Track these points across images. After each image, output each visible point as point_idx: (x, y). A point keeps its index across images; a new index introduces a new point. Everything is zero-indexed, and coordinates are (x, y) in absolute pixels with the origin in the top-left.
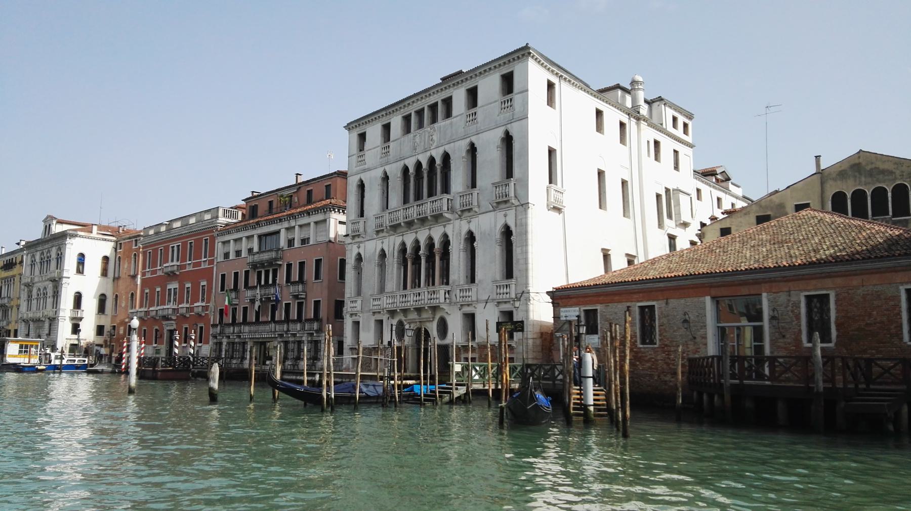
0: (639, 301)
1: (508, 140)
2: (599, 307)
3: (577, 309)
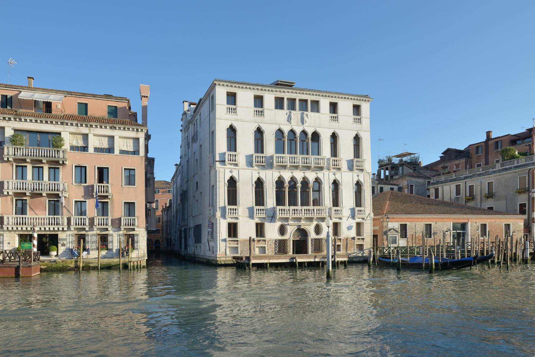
2: (408, 223)
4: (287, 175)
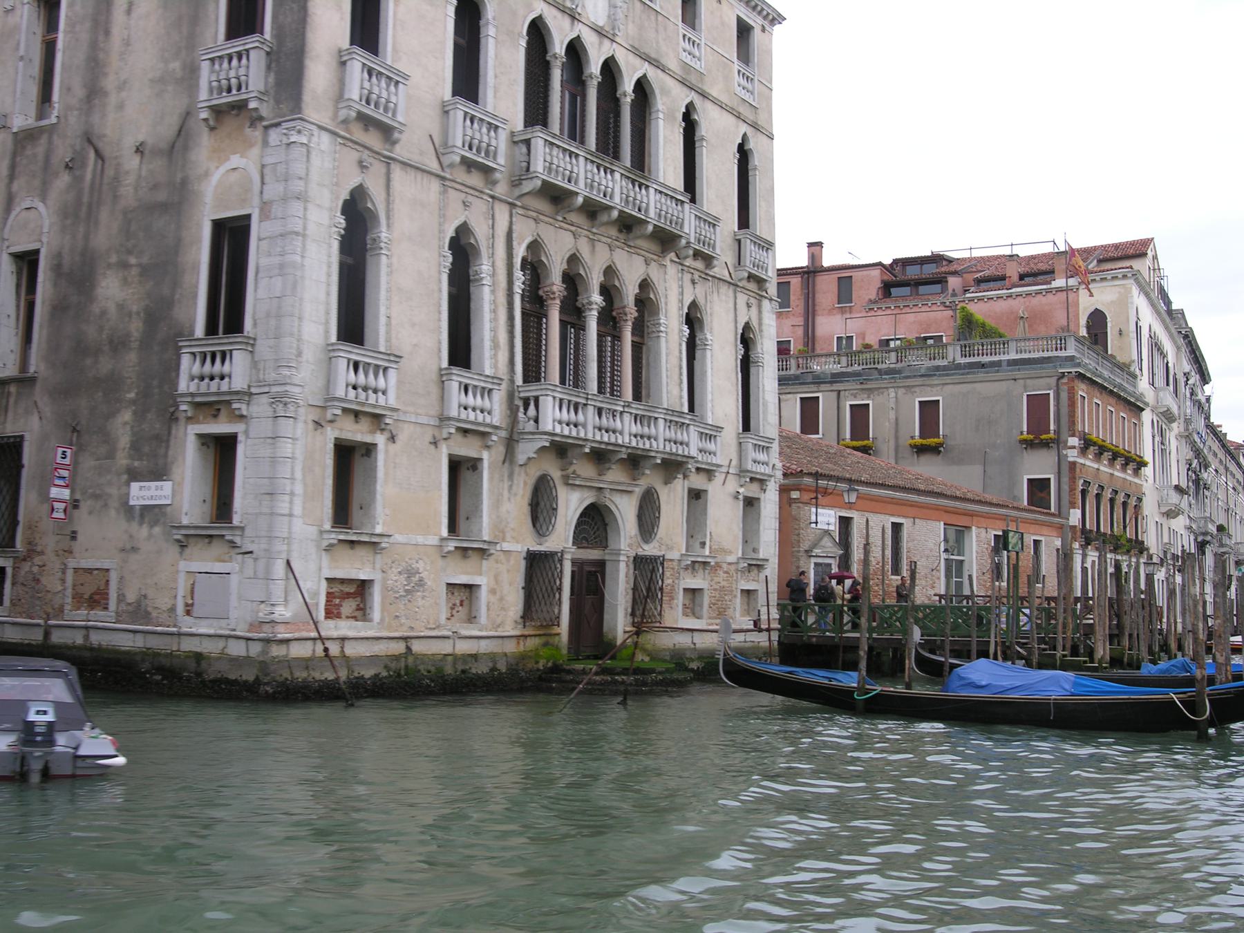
0: (892, 515)
1: (744, 154)
3: (832, 512)
4: (559, 246)
